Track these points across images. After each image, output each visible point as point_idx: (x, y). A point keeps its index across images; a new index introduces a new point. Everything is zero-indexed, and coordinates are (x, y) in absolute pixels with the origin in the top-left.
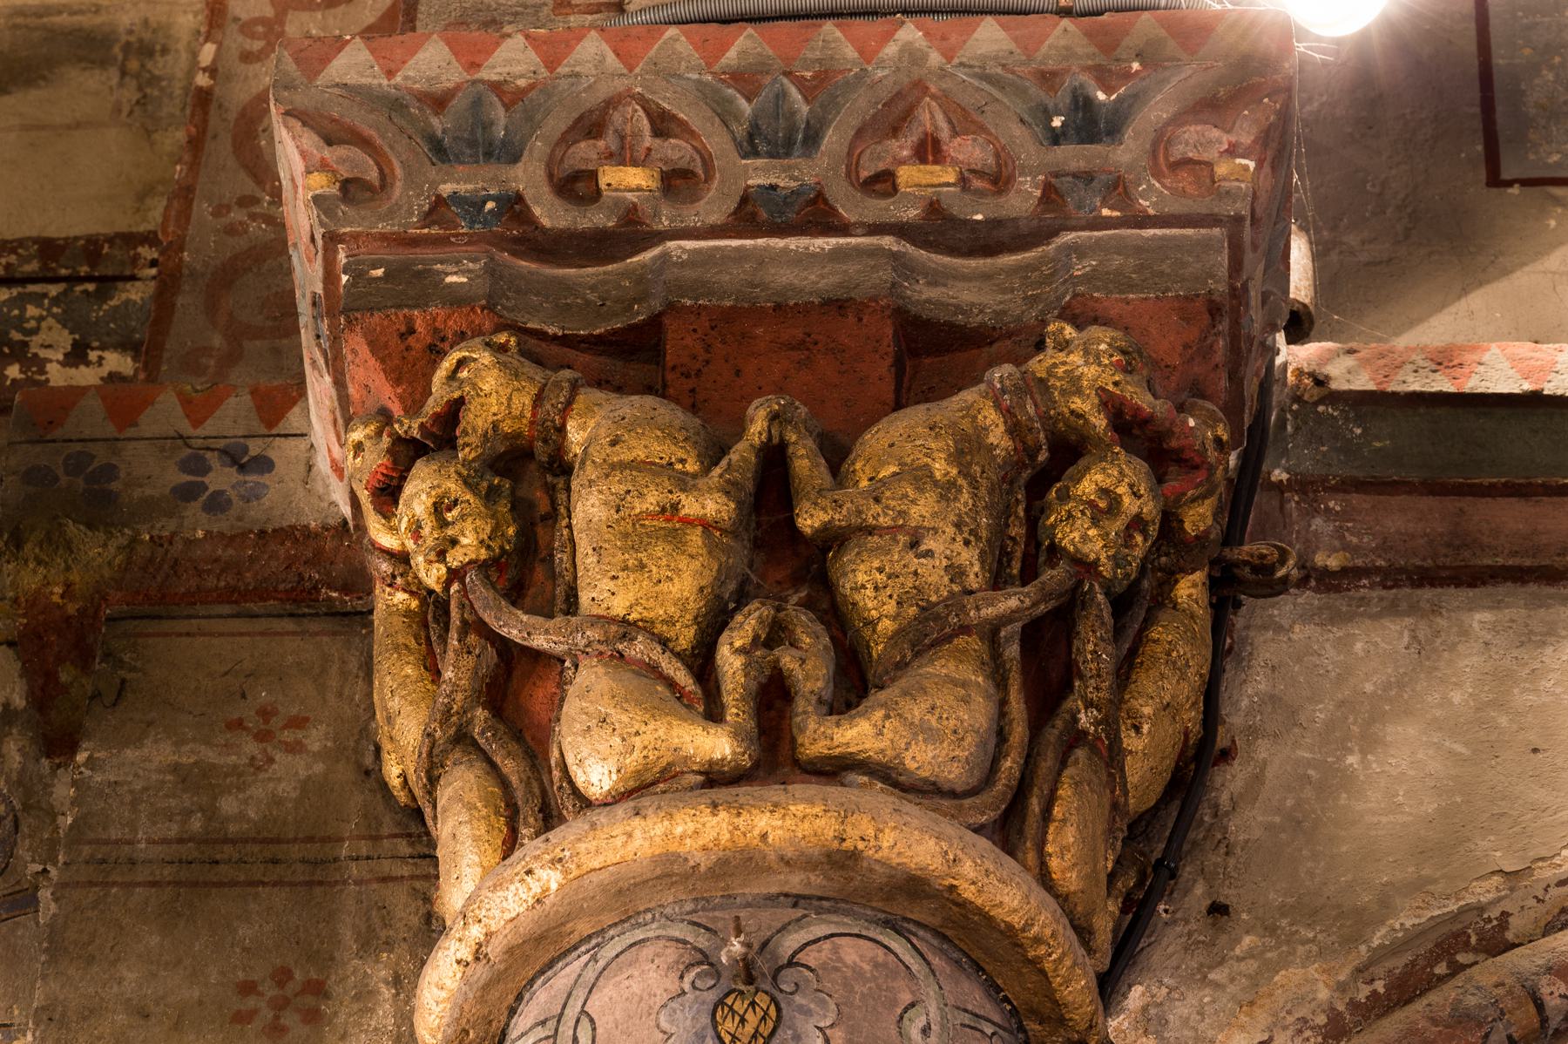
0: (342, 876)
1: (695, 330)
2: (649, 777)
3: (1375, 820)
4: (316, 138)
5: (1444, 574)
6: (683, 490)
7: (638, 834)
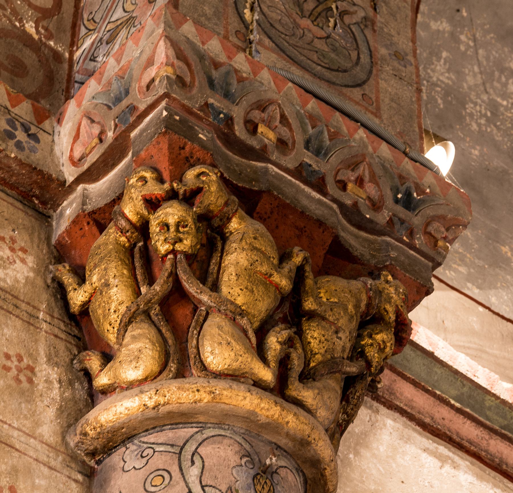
0: (40, 326)
1: (271, 204)
2: (237, 373)
3: (357, 483)
4: (174, 53)
5: (383, 400)
6: (276, 271)
7: (248, 399)
